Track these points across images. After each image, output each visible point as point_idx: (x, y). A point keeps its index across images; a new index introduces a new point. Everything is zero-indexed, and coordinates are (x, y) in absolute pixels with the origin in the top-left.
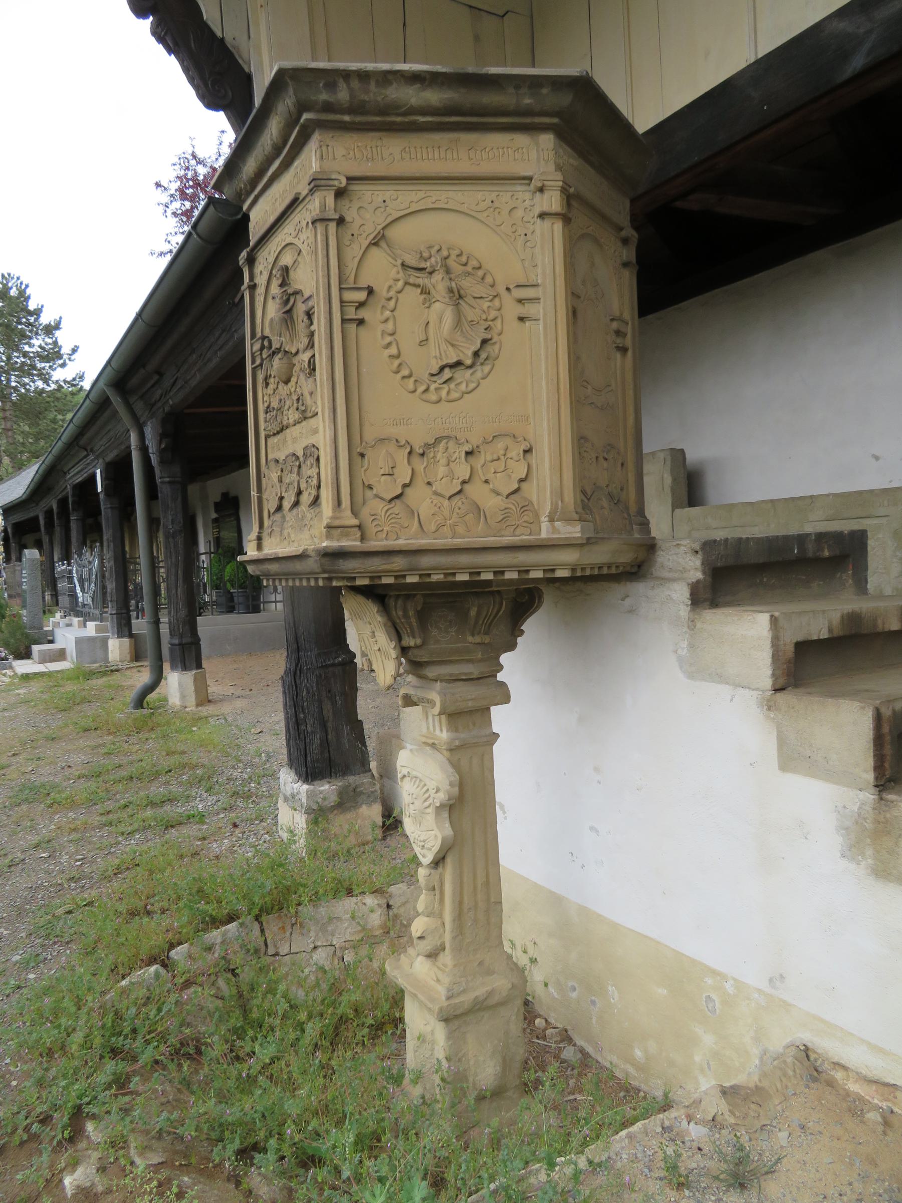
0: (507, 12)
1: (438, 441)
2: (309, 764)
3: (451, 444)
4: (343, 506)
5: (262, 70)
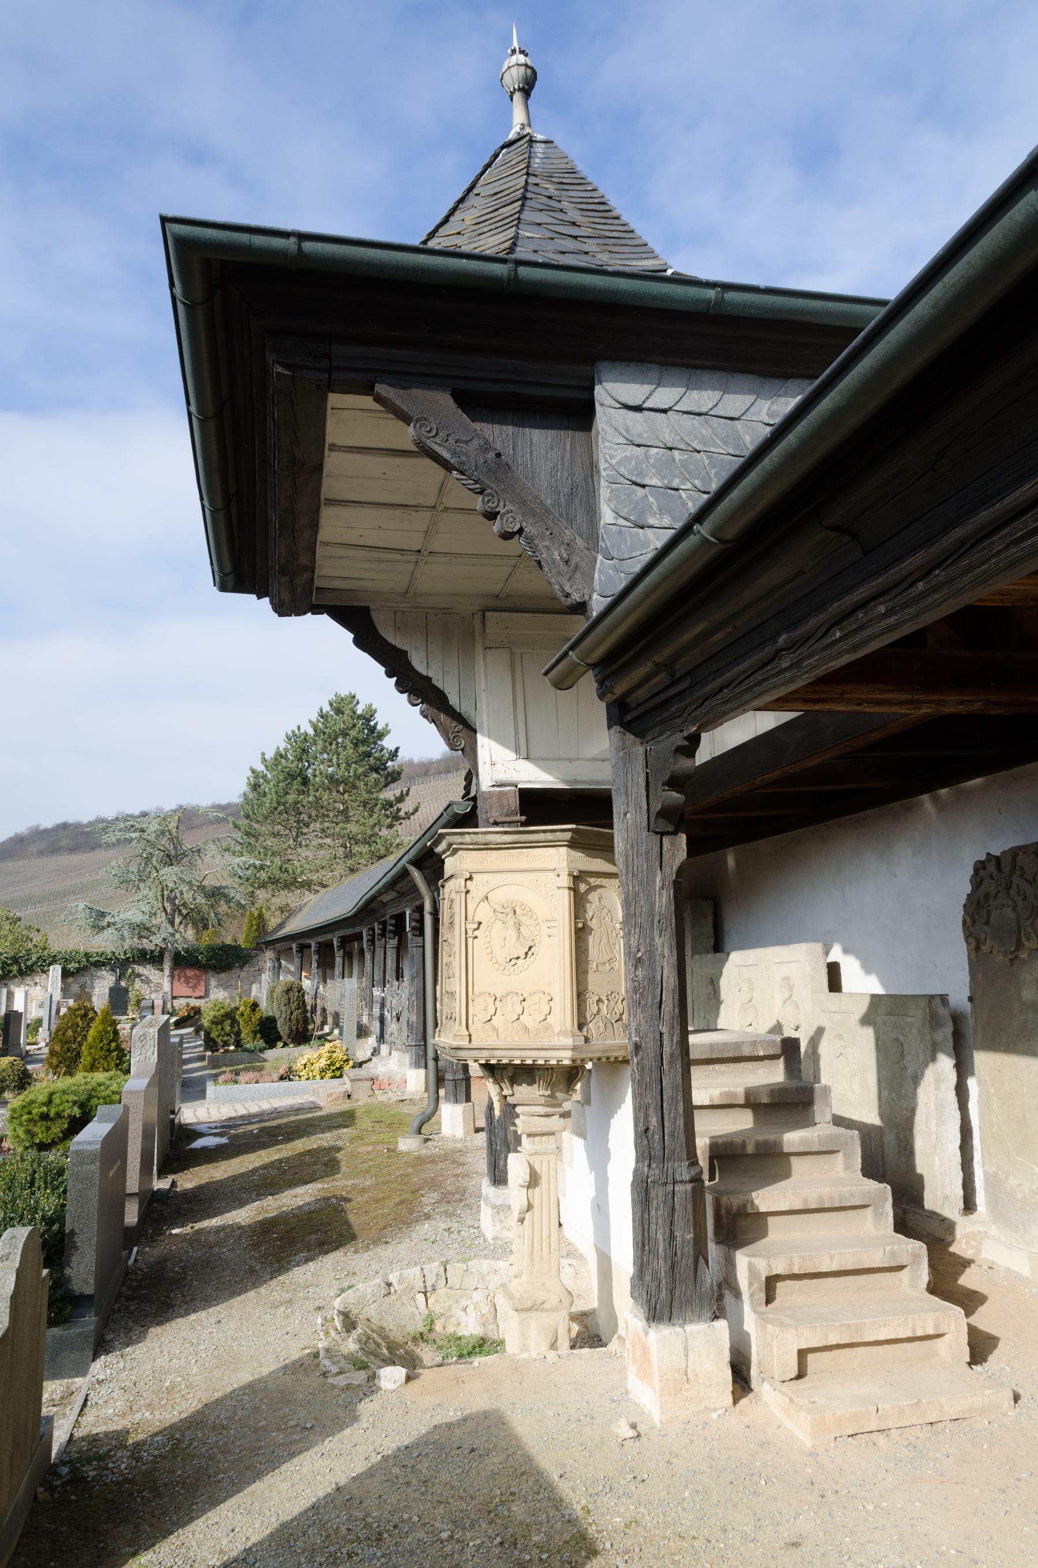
1: (508, 994)
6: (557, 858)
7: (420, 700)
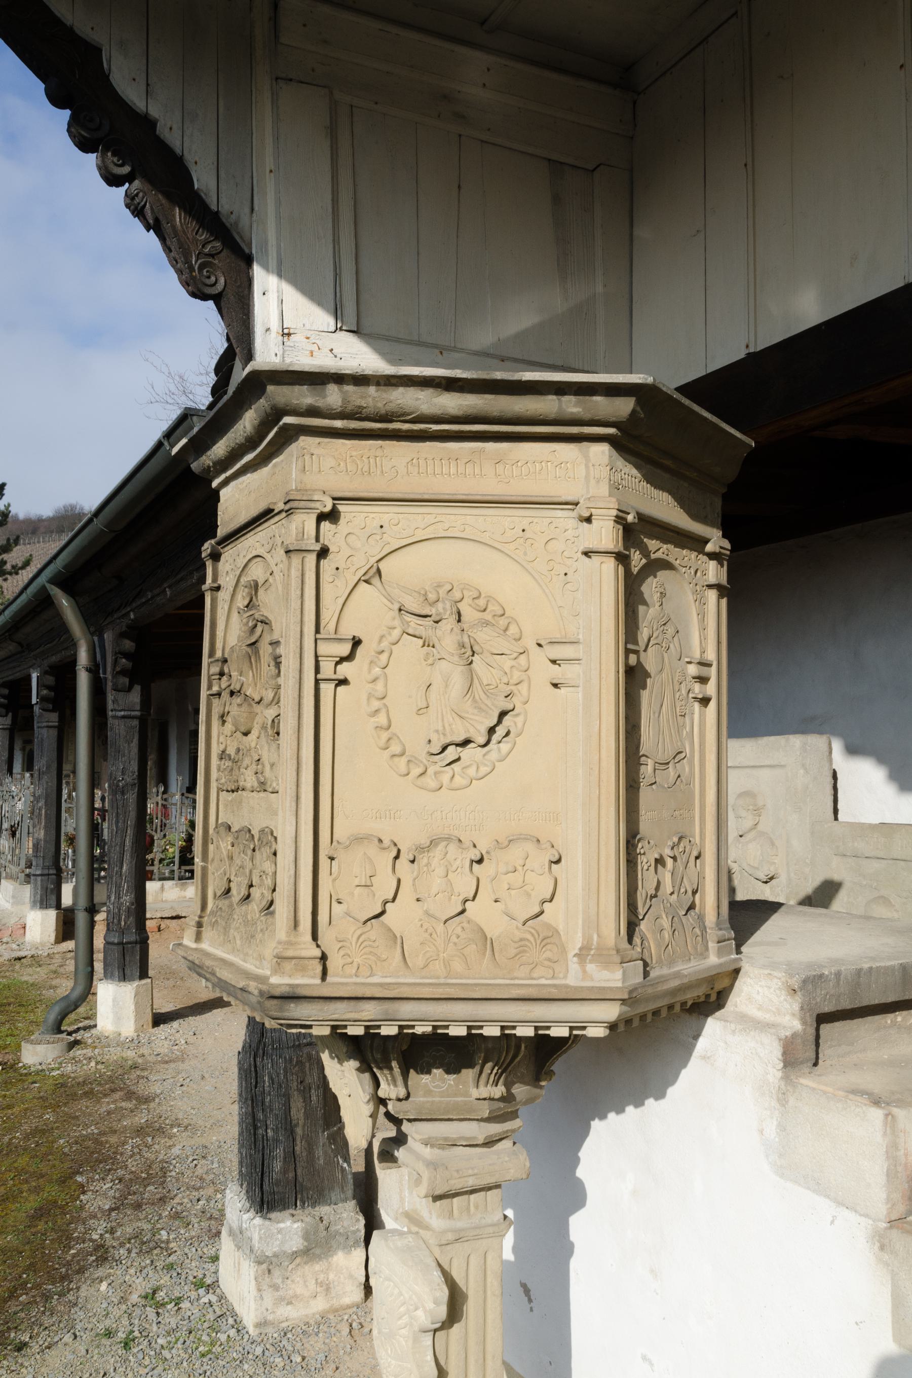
0: (598, 166)
1: (433, 843)
2: (266, 1187)
3: (452, 848)
5: (266, 251)
6: (581, 471)
7: (126, 169)
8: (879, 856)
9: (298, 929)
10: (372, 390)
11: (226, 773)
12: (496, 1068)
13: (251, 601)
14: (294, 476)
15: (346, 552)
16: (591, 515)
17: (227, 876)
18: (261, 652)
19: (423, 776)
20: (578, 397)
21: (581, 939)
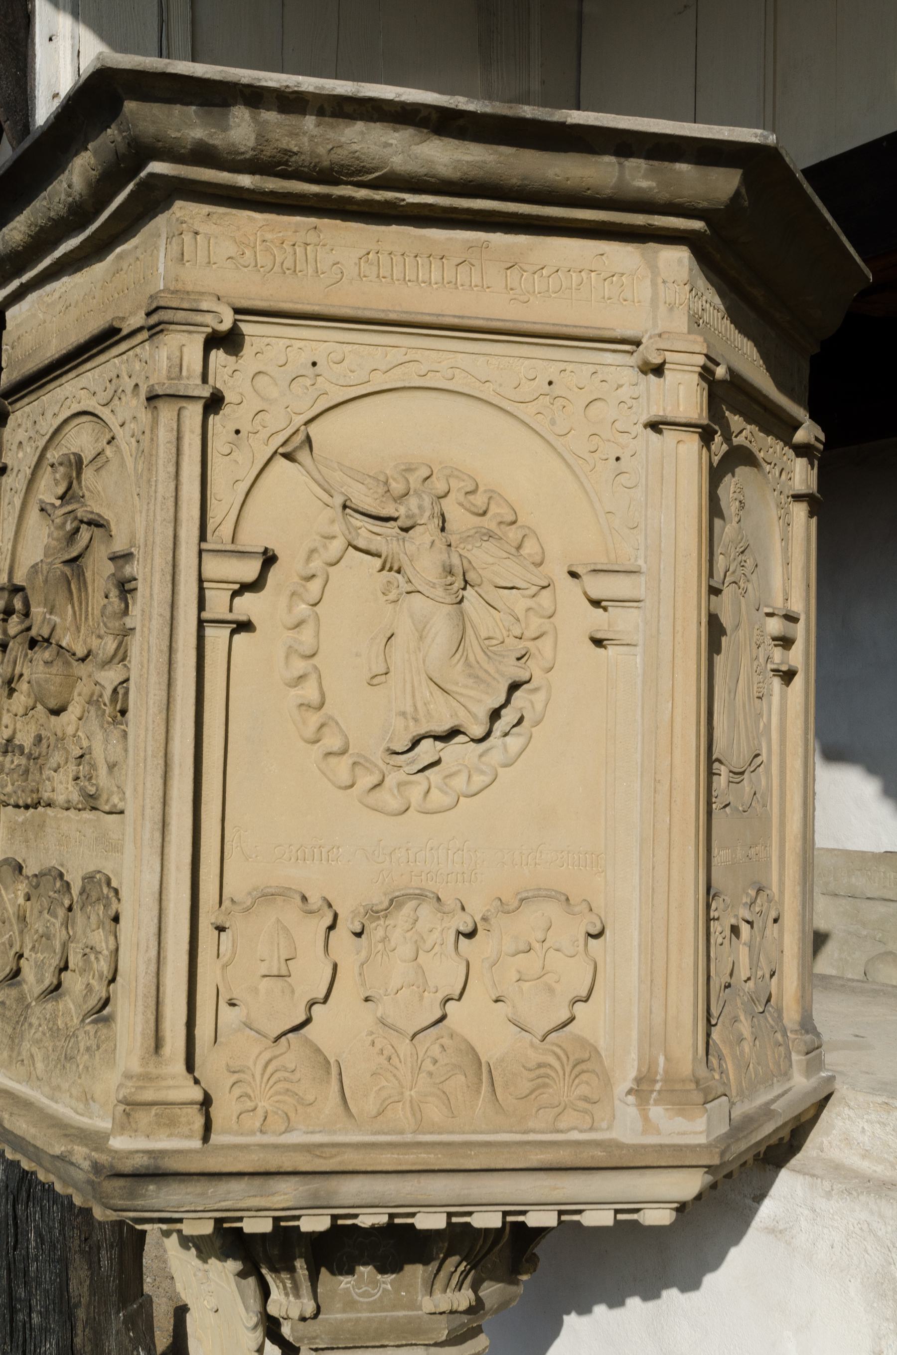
1: (395, 903)
3: (426, 911)
4: (167, 1050)
6: (645, 291)
8: (887, 897)
9: (162, 1052)
10: (309, 122)
11: (15, 776)
12: (464, 1264)
13: (69, 487)
14: (161, 270)
15: (253, 404)
16: (664, 363)
17: (16, 948)
18: (88, 575)
19: (378, 789)
20: (651, 162)
21: (636, 1064)
